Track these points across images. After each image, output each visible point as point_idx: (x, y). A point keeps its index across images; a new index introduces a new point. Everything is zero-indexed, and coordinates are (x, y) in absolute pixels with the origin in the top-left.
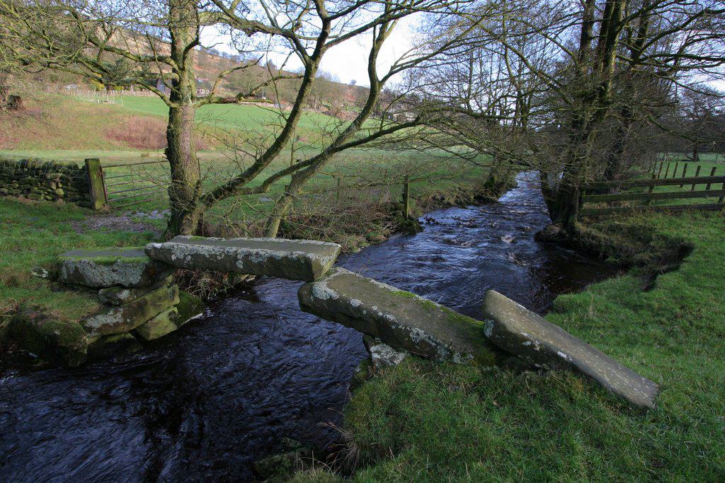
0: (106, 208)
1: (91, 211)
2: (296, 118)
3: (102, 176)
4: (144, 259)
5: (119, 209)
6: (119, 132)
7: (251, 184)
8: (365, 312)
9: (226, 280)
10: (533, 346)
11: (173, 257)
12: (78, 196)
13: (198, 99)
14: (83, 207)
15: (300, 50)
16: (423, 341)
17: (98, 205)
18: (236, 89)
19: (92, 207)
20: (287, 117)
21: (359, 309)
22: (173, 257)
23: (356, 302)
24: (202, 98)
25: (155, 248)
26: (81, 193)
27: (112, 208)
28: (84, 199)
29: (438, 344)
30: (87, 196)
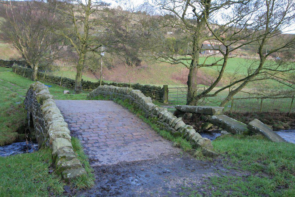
0: (167, 103)
1: (162, 104)
2: (222, 72)
3: (168, 91)
4: (175, 110)
5: (171, 104)
6: (178, 76)
7: (212, 92)
8: (222, 122)
9: (200, 128)
10: (254, 128)
11: (182, 109)
12: (159, 98)
13: (199, 65)
14: (160, 102)
15: (223, 53)
16: (233, 129)
17: (165, 102)
18: (249, 49)
19: (163, 102)
20: (220, 72)
21: (221, 121)
22: (182, 109)
23: (220, 120)
24: (200, 65)
25: (178, 106)
26: (160, 97)
27: (169, 104)
28: (161, 100)
29: (236, 129)
30: (162, 98)
